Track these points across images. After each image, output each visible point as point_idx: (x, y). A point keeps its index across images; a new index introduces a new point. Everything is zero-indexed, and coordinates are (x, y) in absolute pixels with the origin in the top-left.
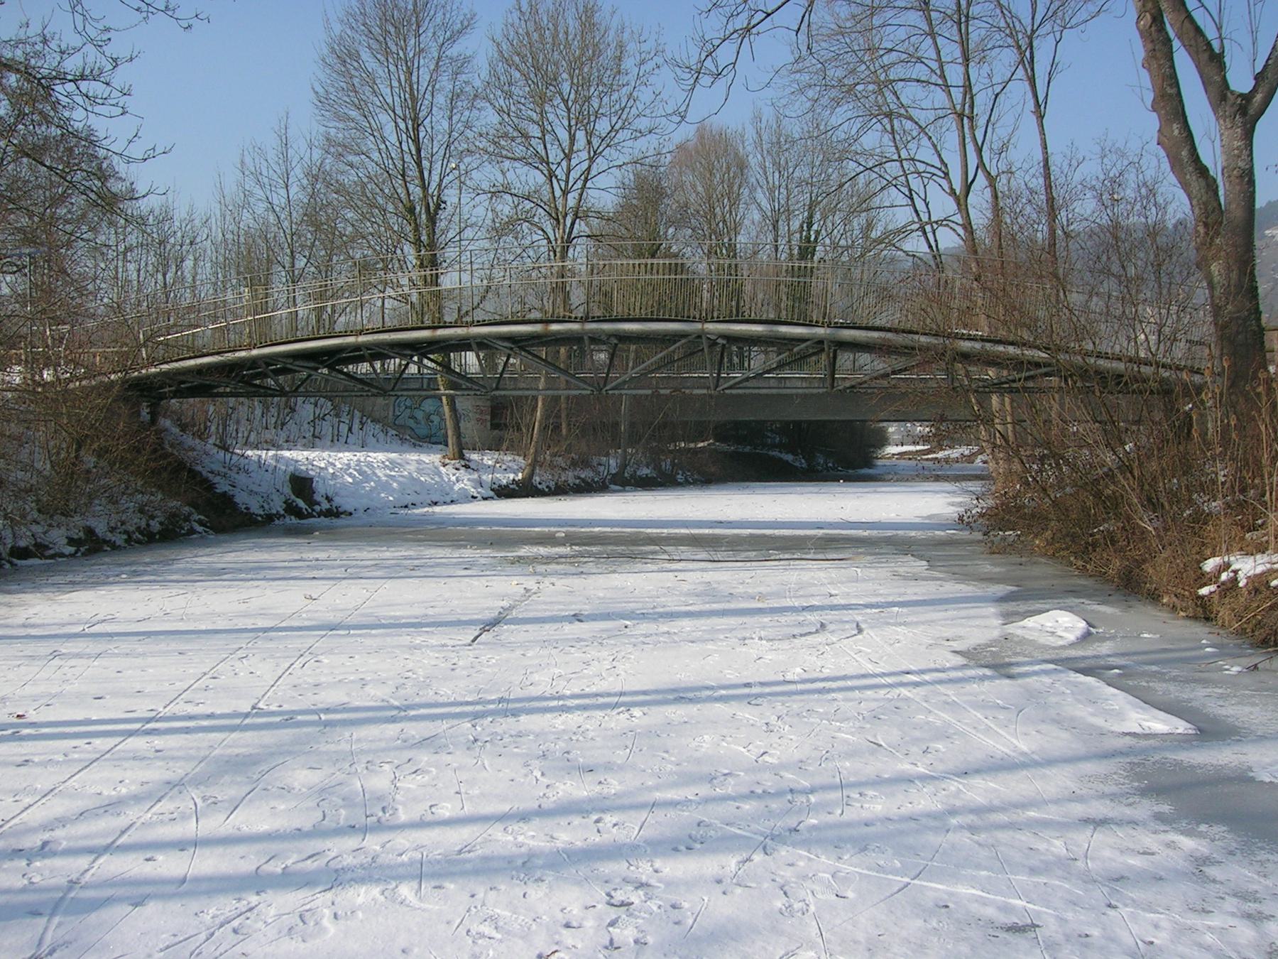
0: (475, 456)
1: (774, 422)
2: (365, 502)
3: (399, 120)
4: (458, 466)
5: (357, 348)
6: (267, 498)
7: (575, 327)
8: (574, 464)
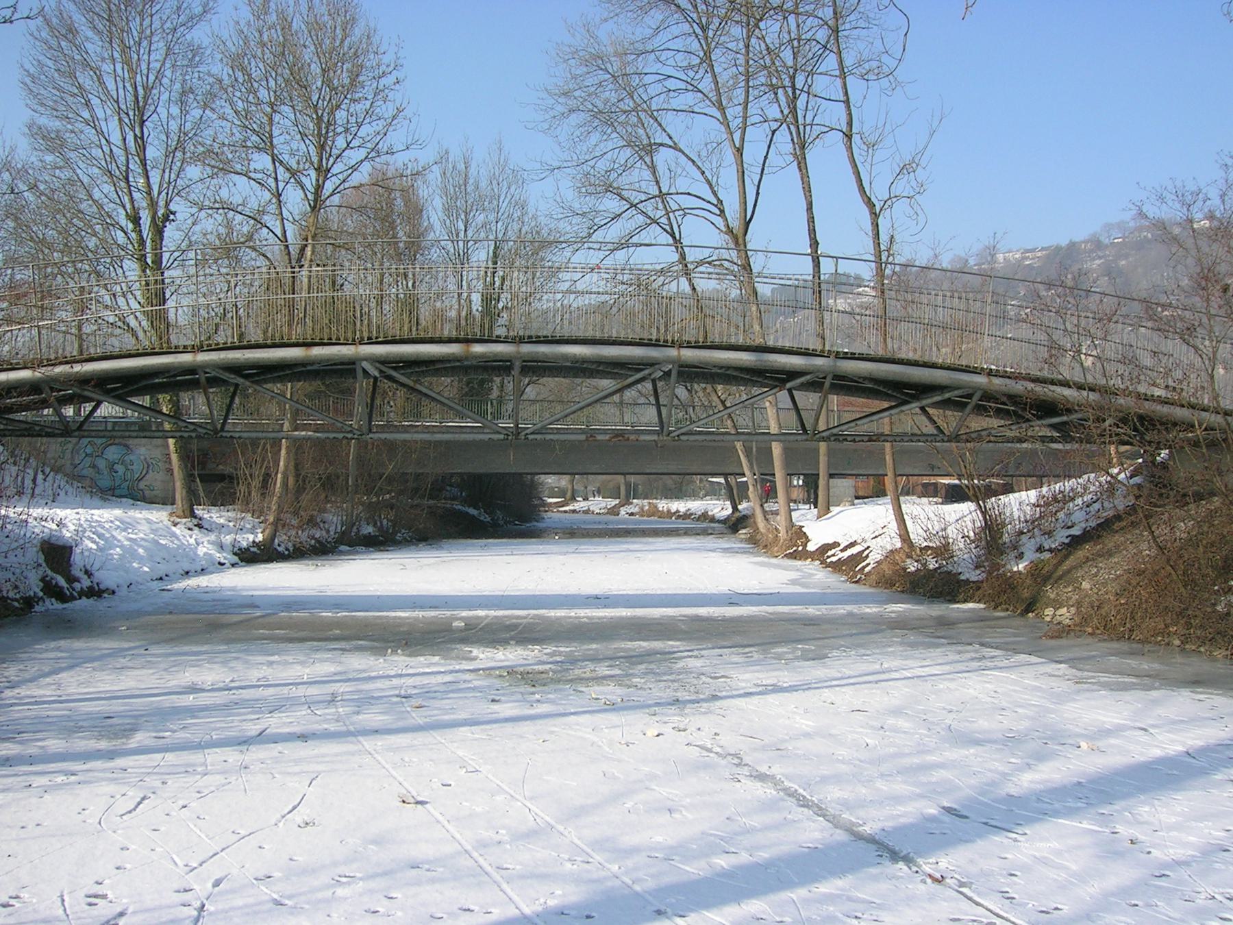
1: (452, 475)
3: (123, 115)
4: (190, 525)
5: (192, 370)
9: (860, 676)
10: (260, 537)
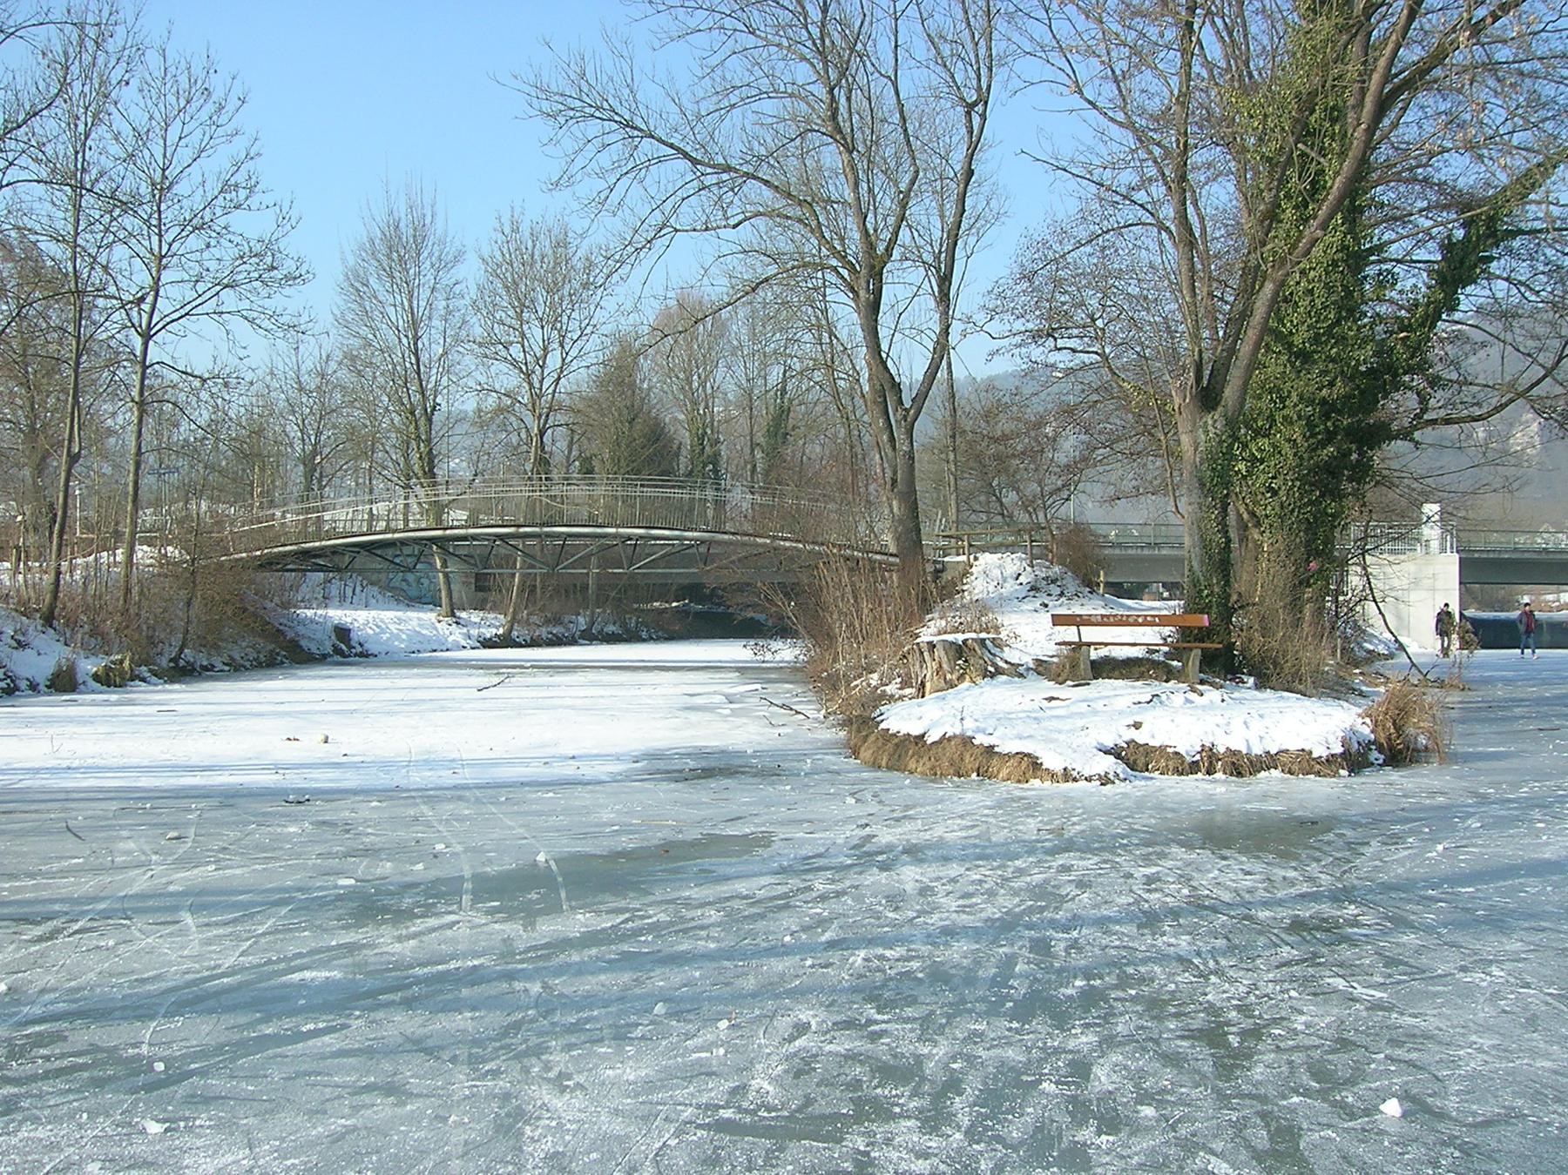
0: (464, 615)
2: (382, 649)
6: (321, 643)
7: (537, 529)
8: (547, 622)
9: (308, 713)
10: (501, 631)
